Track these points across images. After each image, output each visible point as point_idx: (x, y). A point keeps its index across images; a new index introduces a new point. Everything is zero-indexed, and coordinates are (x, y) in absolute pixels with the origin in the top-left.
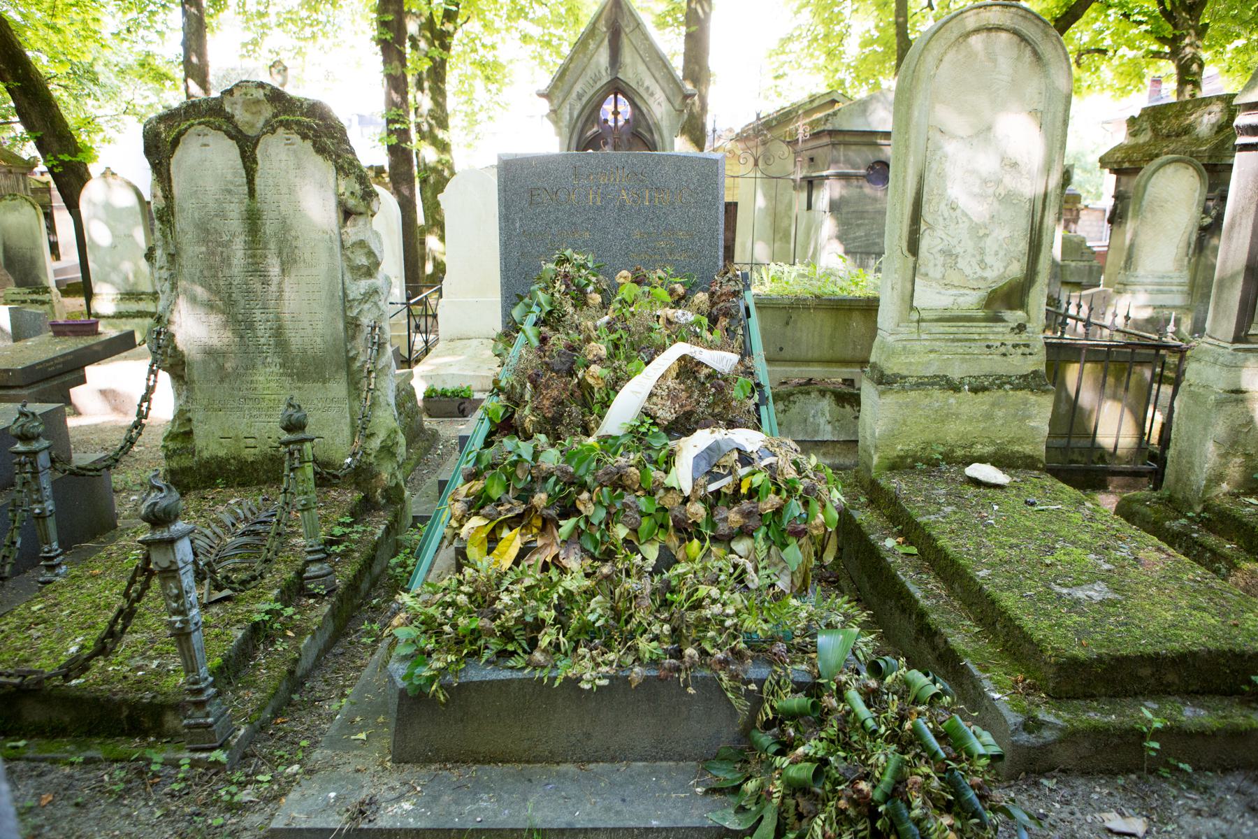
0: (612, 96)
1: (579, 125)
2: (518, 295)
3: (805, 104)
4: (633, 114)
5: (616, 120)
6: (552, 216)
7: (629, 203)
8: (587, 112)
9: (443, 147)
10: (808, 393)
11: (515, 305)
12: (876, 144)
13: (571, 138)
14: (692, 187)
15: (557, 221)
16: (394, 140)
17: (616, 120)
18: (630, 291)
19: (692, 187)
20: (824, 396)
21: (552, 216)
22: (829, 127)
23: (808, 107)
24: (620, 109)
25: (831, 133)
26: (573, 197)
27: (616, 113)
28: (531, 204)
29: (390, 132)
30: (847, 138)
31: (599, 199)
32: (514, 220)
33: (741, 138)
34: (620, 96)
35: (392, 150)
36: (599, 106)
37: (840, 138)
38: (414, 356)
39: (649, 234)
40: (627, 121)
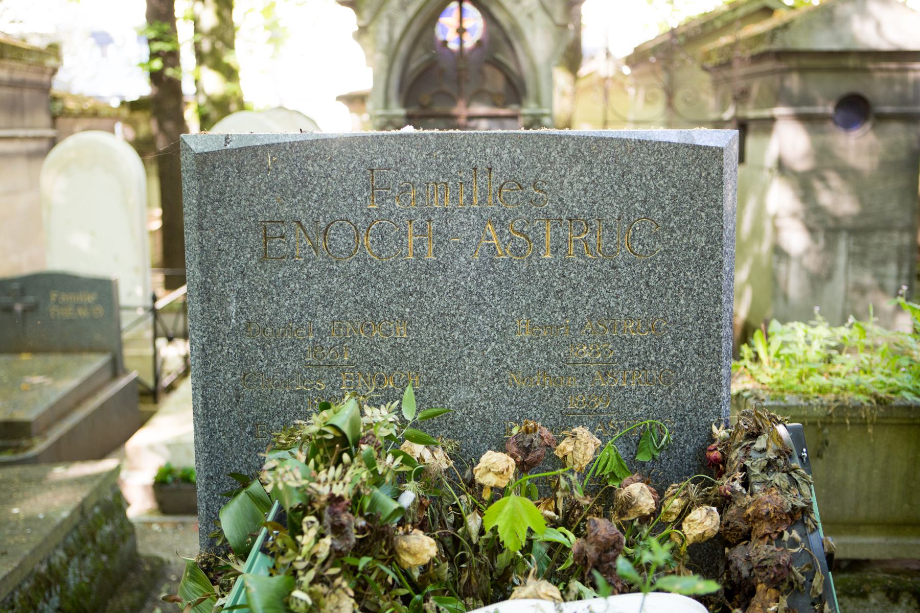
0: (454, 5)
1: (403, 49)
2: (236, 475)
3: (724, 13)
4: (487, 31)
5: (461, 42)
6: (317, 288)
7: (503, 254)
8: (415, 29)
9: (230, 74)
10: (864, 595)
11: (232, 494)
12: (866, 71)
13: (390, 70)
14: (658, 214)
15: (326, 300)
16: (157, 64)
17: (461, 42)
18: (514, 518)
19: (658, 214)
20: (895, 600)
21: (317, 288)
22: (777, 46)
23: (729, 17)
24: (467, 24)
25: (781, 55)
26: (367, 241)
27: (461, 31)
28: (264, 258)
29: (154, 55)
30: (805, 62)
31: (429, 247)
32: (223, 296)
33: (638, 58)
34: (467, 6)
35: (156, 77)
36: (432, 20)
37: (793, 63)
38: (166, 381)
39: (553, 328)
40: (479, 43)
